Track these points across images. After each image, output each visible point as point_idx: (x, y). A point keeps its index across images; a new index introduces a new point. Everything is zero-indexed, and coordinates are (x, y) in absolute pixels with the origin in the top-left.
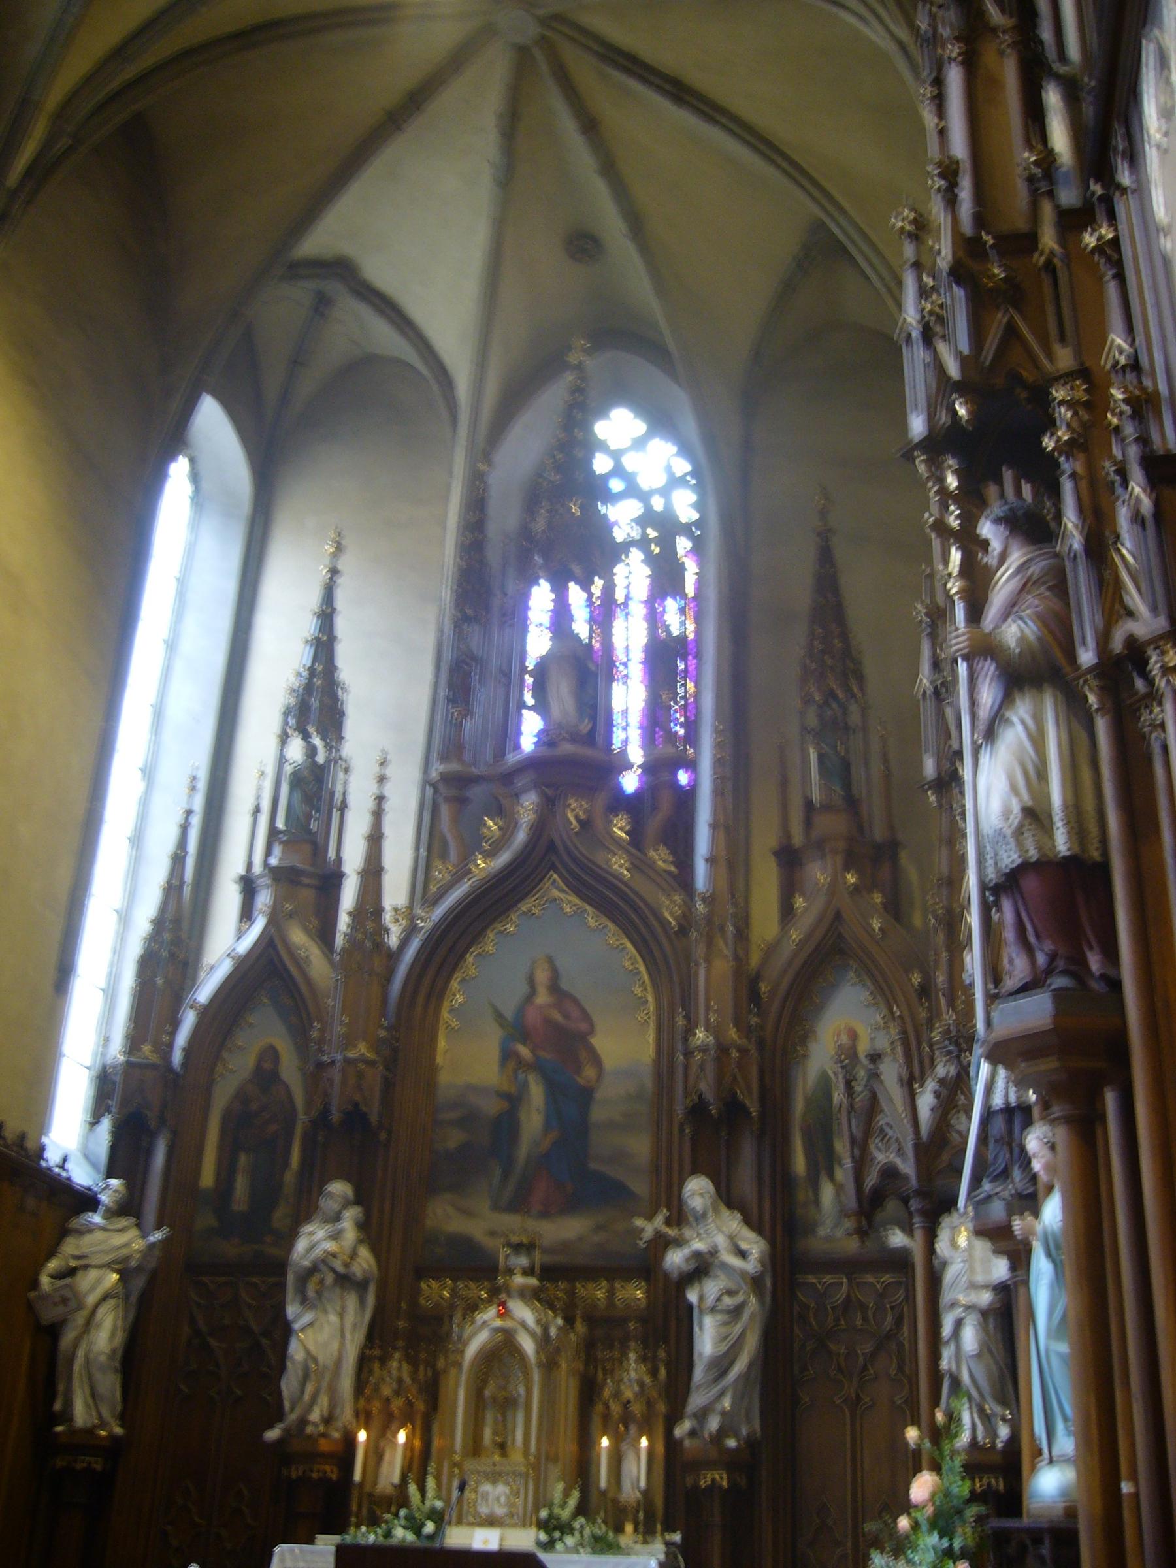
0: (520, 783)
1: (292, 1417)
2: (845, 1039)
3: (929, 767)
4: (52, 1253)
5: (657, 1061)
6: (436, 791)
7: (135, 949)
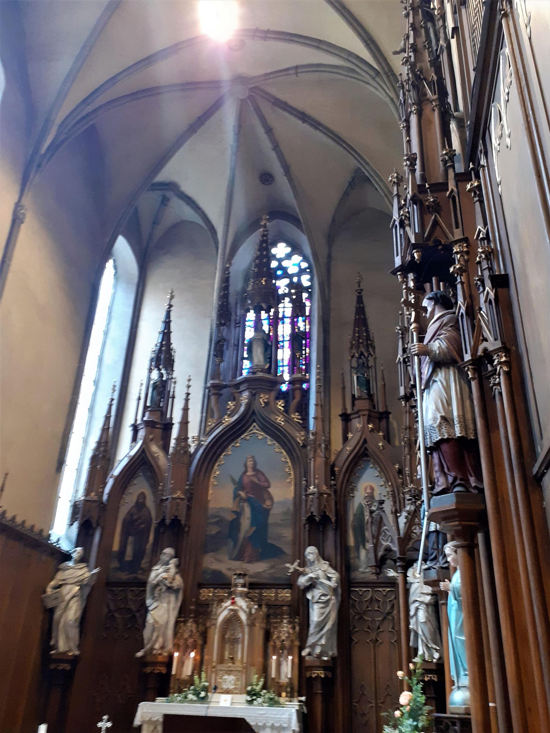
0: (242, 387)
1: (148, 647)
2: (369, 491)
3: (402, 392)
4: (52, 579)
5: (295, 498)
6: (209, 392)
7: (89, 454)
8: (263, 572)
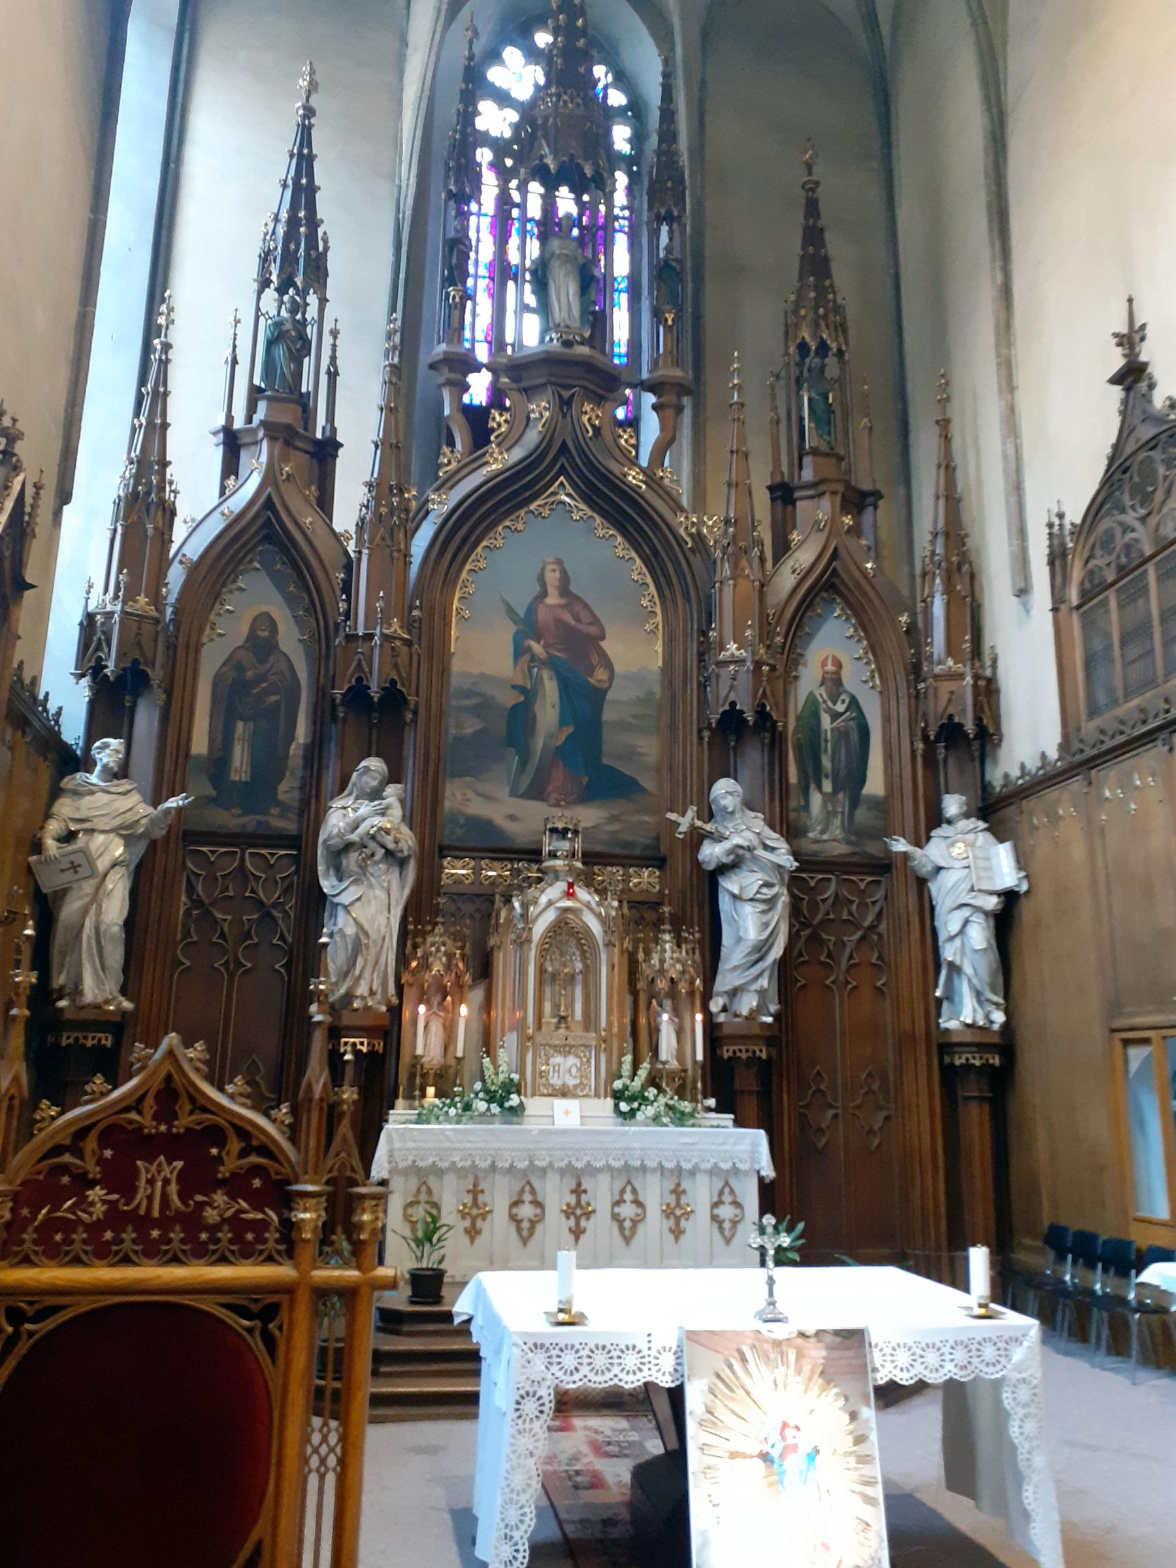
2: (830, 667)
4: (48, 816)
5: (663, 670)
8: (594, 827)
